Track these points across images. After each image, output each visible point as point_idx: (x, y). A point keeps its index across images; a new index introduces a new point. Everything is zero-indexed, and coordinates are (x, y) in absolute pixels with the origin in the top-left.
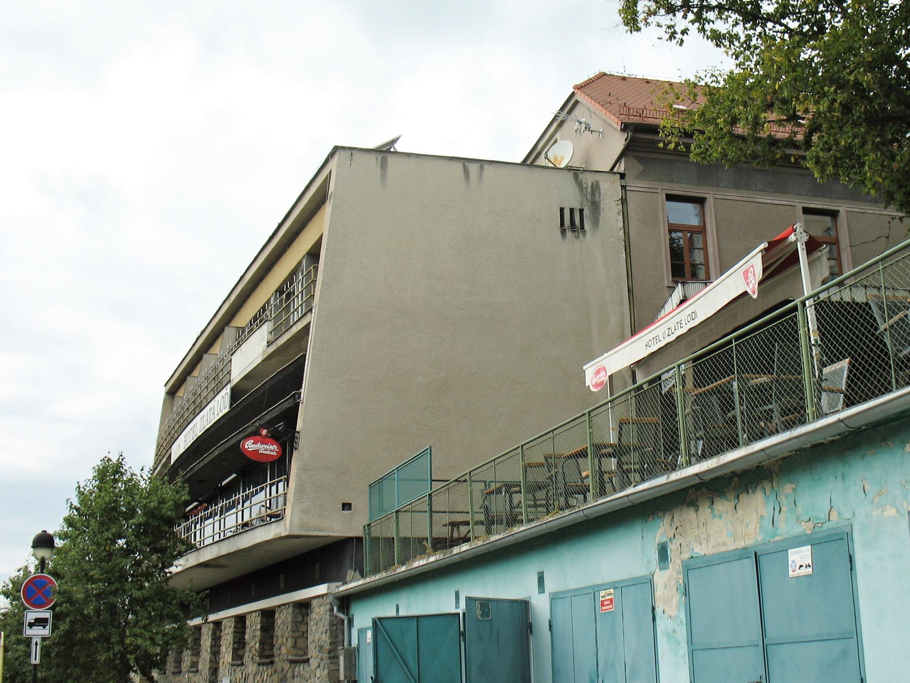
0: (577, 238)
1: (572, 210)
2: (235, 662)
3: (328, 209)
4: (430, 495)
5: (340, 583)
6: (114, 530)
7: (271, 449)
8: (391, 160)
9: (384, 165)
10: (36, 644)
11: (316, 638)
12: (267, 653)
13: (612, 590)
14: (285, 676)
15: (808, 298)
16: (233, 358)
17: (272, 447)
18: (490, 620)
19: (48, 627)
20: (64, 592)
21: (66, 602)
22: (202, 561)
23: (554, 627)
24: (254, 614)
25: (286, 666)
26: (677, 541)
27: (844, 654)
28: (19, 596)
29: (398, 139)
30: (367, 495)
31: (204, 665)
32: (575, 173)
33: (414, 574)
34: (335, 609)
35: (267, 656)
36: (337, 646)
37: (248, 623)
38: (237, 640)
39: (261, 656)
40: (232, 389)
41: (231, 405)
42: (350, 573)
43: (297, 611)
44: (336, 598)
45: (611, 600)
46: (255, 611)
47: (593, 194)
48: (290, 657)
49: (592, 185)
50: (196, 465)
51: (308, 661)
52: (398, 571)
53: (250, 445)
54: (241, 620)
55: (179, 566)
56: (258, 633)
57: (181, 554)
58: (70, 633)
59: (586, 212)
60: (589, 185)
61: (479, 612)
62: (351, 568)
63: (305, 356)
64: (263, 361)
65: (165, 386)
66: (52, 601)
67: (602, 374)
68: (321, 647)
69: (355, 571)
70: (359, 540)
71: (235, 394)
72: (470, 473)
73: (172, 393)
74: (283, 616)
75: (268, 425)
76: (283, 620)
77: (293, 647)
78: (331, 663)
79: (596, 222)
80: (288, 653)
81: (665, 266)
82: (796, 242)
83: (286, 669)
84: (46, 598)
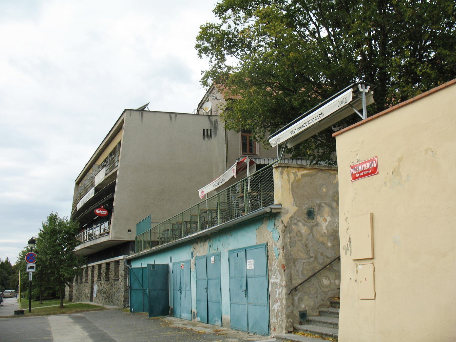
0: (209, 139)
1: (207, 130)
2: (98, 280)
3: (123, 131)
4: (150, 230)
5: (128, 255)
6: (54, 238)
7: (104, 212)
8: (144, 113)
9: (142, 115)
10: (31, 274)
11: (121, 273)
12: (108, 277)
13: (183, 263)
14: (113, 284)
15: (248, 177)
16: (95, 177)
17: (105, 212)
18: (156, 270)
19: (34, 269)
20: (39, 258)
21: (40, 261)
22: (86, 246)
23: (173, 272)
24: (104, 264)
25: (113, 281)
26: (195, 252)
27: (218, 282)
28: (25, 259)
29: (148, 104)
30: (136, 227)
31: (89, 281)
32: (209, 117)
33: (154, 251)
34: (126, 263)
35: (107, 278)
36: (126, 275)
37: (102, 267)
38: (99, 272)
39: (106, 278)
40: (95, 188)
41: (95, 193)
42: (131, 252)
43: (116, 264)
44: (126, 260)
45: (183, 266)
46: (104, 263)
47: (215, 124)
48: (114, 278)
49: (215, 121)
50: (84, 213)
51: (118, 280)
52: (140, 253)
53: (98, 211)
54: (100, 265)
55: (78, 248)
56: (105, 270)
57: (78, 245)
58: (42, 271)
59: (212, 130)
60: (214, 121)
61: (151, 268)
62: (131, 251)
63: (116, 181)
64: (104, 180)
65: (75, 181)
66: (35, 261)
67: (203, 193)
68: (122, 276)
69: (132, 251)
70: (134, 241)
71: (96, 190)
72: (183, 213)
73: (78, 183)
74: (112, 265)
75: (102, 204)
76: (112, 266)
77: (114, 275)
78: (125, 280)
79: (216, 134)
80: (113, 277)
81: (240, 149)
82: (246, 162)
83: (113, 282)
84: (34, 260)
